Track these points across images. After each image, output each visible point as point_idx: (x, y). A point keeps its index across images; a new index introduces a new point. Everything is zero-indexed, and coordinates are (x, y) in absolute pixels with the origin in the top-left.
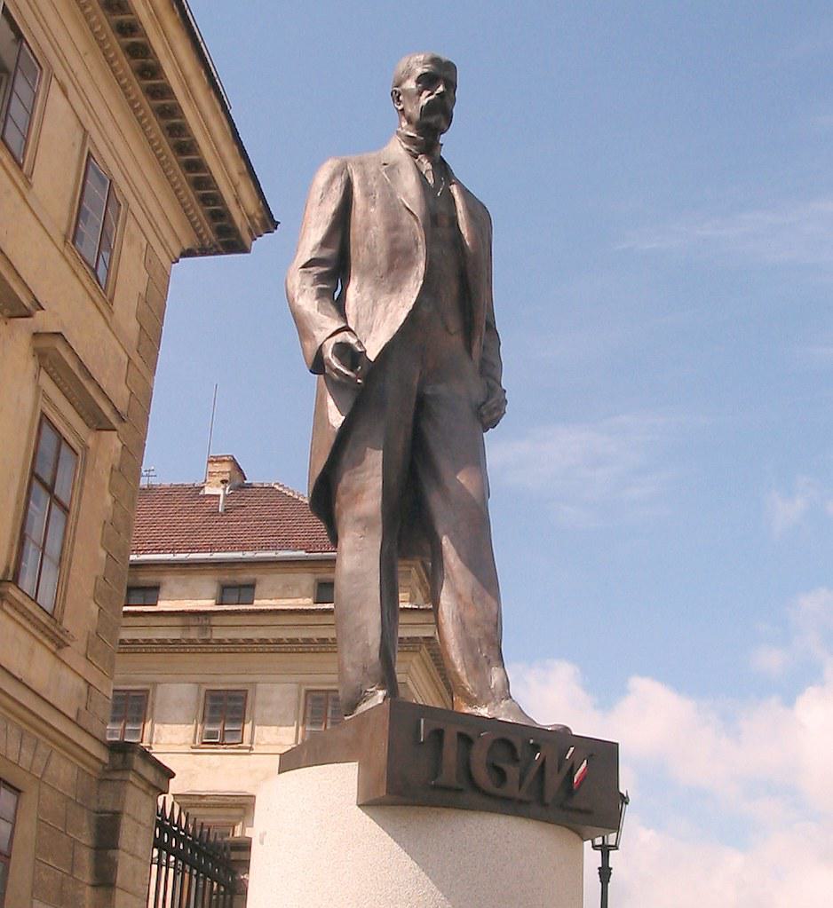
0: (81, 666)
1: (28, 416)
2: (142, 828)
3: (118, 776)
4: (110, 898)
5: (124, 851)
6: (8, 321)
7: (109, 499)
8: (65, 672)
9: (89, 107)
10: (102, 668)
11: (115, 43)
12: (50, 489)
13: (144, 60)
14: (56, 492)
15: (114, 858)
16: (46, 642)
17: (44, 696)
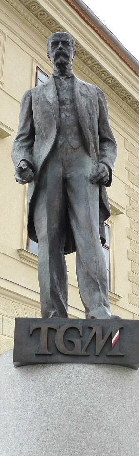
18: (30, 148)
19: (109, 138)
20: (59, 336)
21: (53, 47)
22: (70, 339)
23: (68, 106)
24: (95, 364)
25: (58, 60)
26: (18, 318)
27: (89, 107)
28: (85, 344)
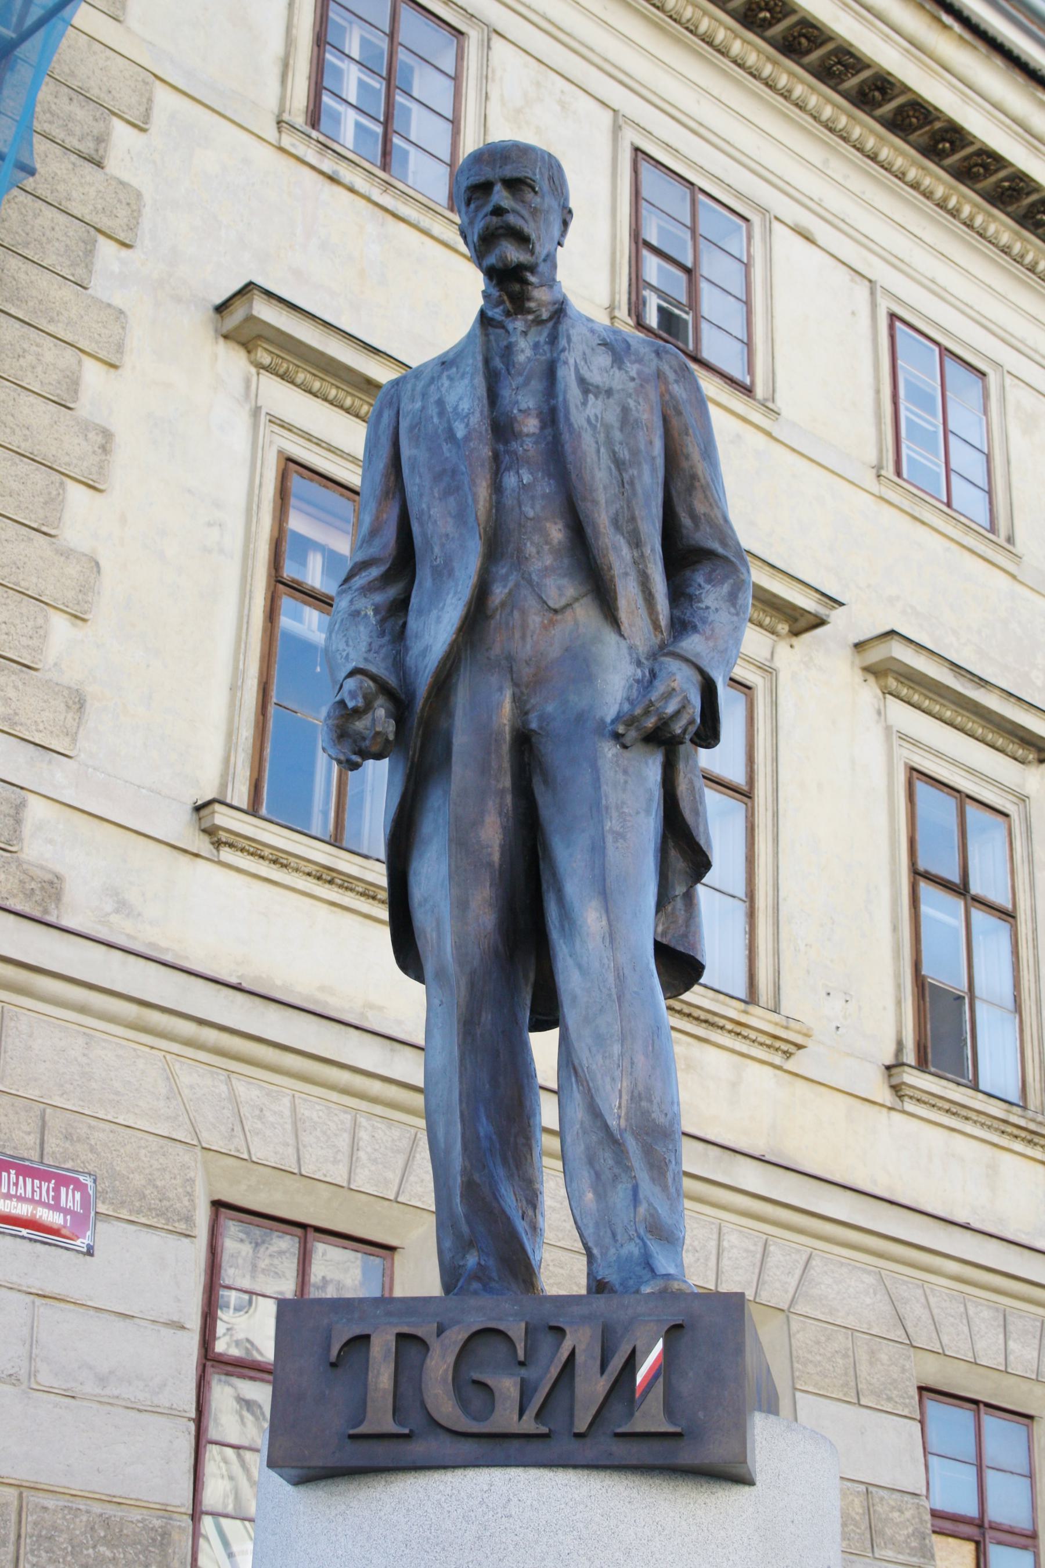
1: (880, 781)
6: (795, 641)
9: (865, 242)
11: (865, 128)
12: (960, 889)
13: (927, 128)
14: (976, 888)
16: (1018, 1146)
19: (720, 550)
20: (439, 1365)
21: (472, 206)
22: (477, 1376)
24: (575, 1467)
25: (491, 260)
26: (339, 1299)
27: (617, 435)
28: (535, 1390)
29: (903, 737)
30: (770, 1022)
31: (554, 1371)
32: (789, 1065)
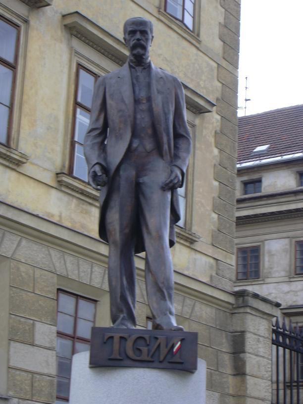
0: (210, 251)
2: (261, 339)
3: (241, 310)
4: (244, 382)
5: (249, 353)
7: (216, 151)
8: (198, 256)
10: (225, 249)
15: (244, 358)
17: (186, 273)
18: (102, 148)
19: (184, 134)
22: (138, 347)
23: (144, 106)
25: (135, 52)
29: (76, 52)
30: (14, 153)
31: (155, 347)
32: (192, 246)
